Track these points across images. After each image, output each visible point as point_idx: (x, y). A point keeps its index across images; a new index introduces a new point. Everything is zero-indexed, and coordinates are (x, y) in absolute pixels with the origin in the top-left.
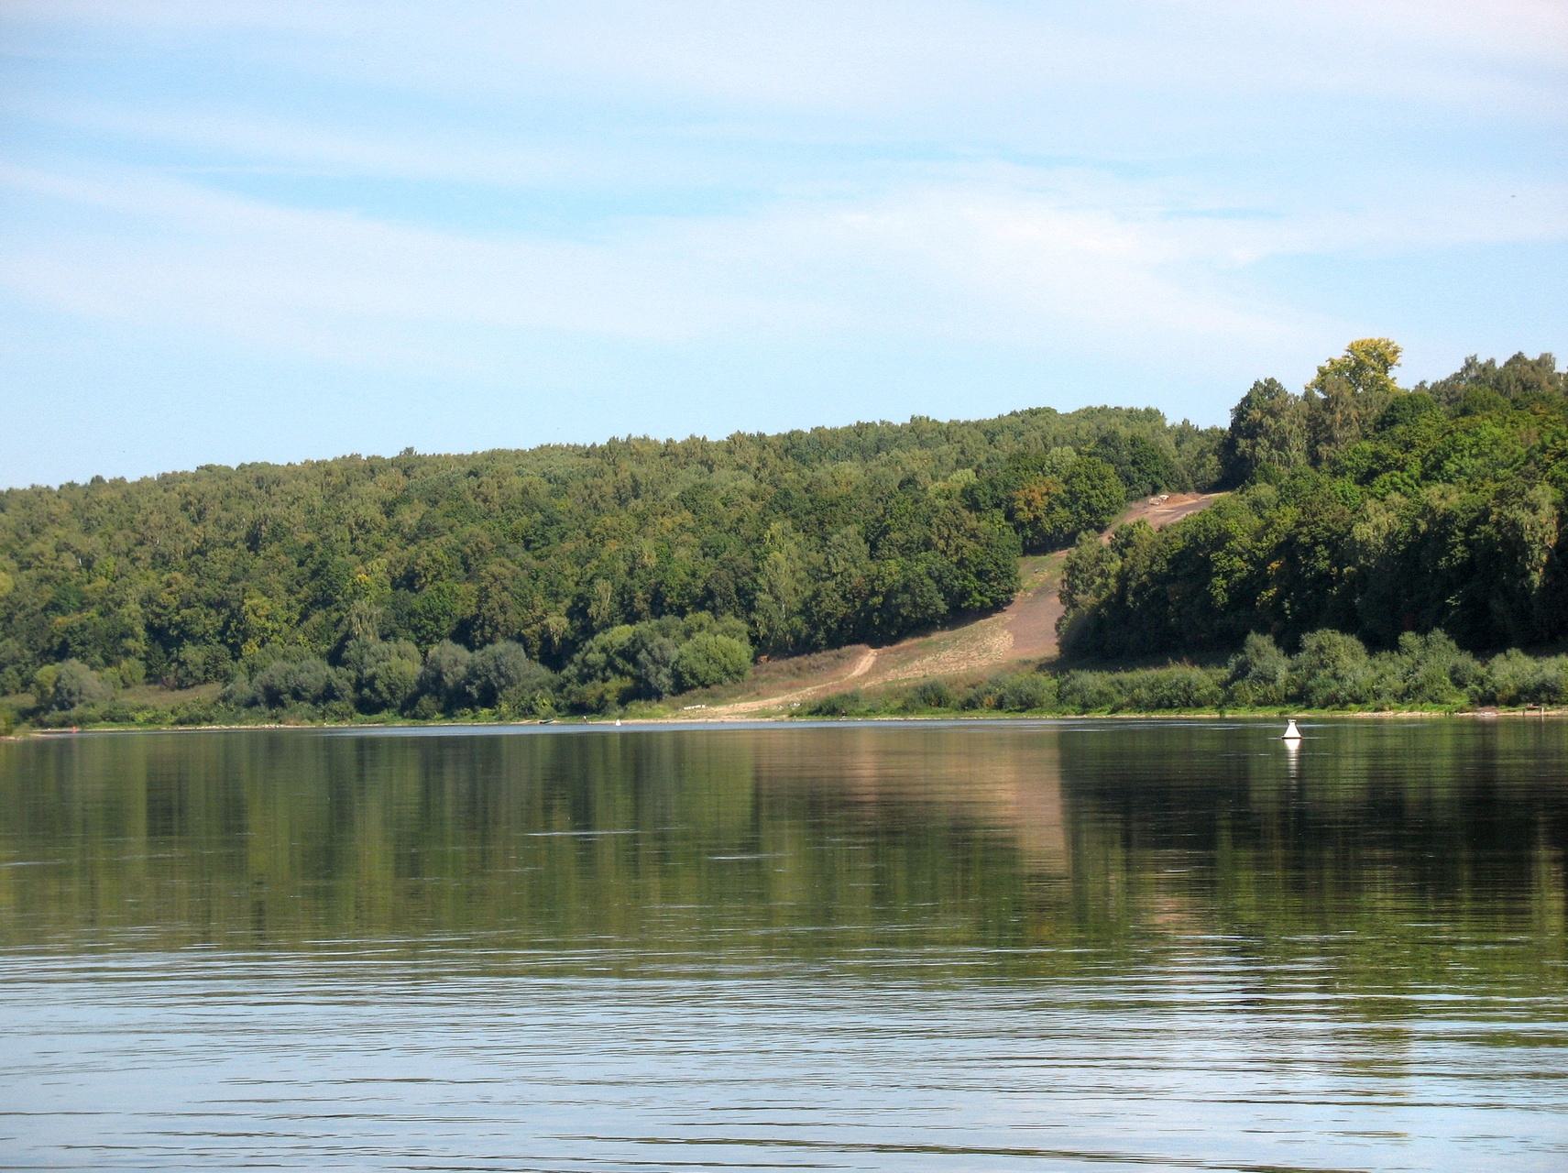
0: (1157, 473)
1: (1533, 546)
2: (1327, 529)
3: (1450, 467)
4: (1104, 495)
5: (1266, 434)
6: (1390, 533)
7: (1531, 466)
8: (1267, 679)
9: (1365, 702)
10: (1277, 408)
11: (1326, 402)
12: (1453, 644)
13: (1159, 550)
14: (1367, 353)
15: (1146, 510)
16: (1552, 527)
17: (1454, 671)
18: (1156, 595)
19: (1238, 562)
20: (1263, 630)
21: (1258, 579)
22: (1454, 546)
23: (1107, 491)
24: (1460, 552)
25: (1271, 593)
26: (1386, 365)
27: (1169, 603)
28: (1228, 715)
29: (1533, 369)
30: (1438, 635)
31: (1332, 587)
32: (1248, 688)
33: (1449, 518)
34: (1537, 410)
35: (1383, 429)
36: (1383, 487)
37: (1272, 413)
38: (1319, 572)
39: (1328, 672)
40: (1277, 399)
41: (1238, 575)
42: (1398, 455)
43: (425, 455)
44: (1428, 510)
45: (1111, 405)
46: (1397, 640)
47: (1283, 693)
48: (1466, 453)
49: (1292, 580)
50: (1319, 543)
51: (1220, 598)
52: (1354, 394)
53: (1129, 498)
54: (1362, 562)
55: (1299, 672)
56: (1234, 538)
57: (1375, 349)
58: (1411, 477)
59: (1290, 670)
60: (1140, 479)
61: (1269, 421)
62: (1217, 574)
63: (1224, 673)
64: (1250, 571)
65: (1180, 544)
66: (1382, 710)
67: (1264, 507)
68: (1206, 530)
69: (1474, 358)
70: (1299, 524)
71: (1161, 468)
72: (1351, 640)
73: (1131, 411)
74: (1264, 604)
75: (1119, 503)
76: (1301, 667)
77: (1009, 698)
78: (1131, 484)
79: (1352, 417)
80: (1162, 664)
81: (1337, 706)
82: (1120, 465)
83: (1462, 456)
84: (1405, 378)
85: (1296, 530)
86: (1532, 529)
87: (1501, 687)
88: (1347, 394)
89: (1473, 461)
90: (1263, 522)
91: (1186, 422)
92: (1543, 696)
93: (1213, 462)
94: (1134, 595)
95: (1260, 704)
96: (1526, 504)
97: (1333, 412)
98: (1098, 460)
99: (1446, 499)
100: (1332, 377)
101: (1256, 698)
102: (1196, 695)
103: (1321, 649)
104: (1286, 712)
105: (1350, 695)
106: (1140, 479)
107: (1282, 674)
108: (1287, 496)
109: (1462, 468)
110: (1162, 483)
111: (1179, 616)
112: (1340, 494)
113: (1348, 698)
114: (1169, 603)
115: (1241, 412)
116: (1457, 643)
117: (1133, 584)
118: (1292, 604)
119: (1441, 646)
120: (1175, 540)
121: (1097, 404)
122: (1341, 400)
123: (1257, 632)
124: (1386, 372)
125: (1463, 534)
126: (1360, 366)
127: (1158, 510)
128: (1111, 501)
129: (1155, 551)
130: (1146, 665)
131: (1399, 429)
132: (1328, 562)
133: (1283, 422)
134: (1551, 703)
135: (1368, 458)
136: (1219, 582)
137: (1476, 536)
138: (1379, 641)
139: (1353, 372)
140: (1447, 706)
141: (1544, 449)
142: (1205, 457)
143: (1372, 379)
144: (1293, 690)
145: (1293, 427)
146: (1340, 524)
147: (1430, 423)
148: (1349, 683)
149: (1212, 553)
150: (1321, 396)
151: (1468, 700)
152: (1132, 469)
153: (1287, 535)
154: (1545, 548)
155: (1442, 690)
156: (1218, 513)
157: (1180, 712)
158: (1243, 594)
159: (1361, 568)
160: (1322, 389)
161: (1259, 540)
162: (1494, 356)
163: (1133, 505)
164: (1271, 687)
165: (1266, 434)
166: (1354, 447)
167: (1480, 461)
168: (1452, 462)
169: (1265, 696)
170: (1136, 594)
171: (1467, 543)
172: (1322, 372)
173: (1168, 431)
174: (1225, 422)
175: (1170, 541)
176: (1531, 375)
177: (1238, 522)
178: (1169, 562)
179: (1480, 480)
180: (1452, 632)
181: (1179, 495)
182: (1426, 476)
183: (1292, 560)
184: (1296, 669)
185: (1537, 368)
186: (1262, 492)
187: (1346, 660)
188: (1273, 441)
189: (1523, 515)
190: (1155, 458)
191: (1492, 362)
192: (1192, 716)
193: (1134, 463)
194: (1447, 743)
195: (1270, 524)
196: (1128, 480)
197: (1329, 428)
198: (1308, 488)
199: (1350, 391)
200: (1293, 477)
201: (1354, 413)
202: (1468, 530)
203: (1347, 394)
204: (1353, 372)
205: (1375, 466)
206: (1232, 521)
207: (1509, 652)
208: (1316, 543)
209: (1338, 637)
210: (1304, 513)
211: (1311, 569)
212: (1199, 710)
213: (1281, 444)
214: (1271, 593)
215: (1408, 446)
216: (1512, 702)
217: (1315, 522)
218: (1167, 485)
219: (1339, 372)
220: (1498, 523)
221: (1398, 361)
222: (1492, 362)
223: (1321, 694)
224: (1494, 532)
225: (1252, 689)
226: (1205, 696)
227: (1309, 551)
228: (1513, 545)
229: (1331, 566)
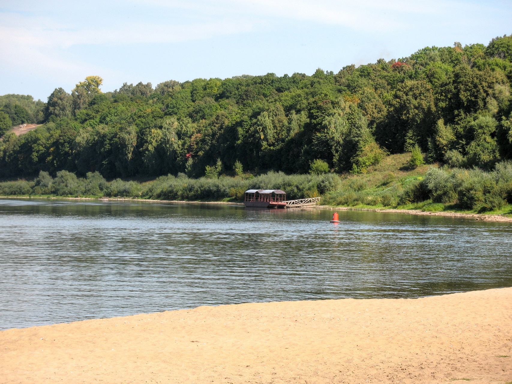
1: (129, 146)
2: (68, 138)
3: (108, 119)
4: (5, 124)
5: (59, 106)
6: (87, 140)
7: (131, 120)
8: (45, 186)
9: (73, 194)
10: (62, 97)
11: (78, 96)
12: (102, 176)
13: (17, 143)
14: (92, 80)
15: (19, 129)
16: (135, 139)
17: (100, 185)
18: (15, 157)
19: (41, 148)
20: (44, 170)
21: (47, 154)
22: (106, 145)
23: (6, 123)
24: (108, 147)
25: (51, 158)
26: (98, 85)
28: (32, 197)
29: (145, 87)
30: (97, 173)
31: (69, 157)
33: (104, 136)
34: (138, 101)
35: (91, 105)
36: (87, 125)
37: (61, 99)
38: (66, 152)
39: (64, 184)
40: (62, 94)
41: (41, 152)
42: (94, 114)
43: (116, 91)
44: (98, 133)
45: (16, 94)
46: (86, 174)
47: (50, 190)
48: (113, 115)
49: (57, 154)
50: (66, 142)
53: (13, 125)
55: (56, 184)
56: (40, 140)
57: (94, 79)
58: (96, 122)
59: (53, 183)
60: (17, 119)
61: (59, 101)
62: (34, 151)
63: (32, 183)
64: (45, 151)
65: (23, 141)
66: (77, 197)
68: (31, 137)
69: (126, 84)
71: (24, 115)
73: (22, 96)
74: (48, 162)
75: (9, 127)
76: (56, 182)
78: (15, 120)
79: (86, 101)
80: (16, 180)
81: (65, 195)
82: (11, 114)
84: (105, 89)
85: (59, 138)
86: (128, 140)
88: (85, 93)
89: (115, 118)
90: (50, 135)
91: (39, 100)
92: (125, 194)
93: (41, 114)
94: (8, 157)
95: (43, 194)
96: (127, 132)
97: (80, 99)
98: (3, 112)
99: (104, 129)
100: (80, 88)
102: (23, 191)
103: (62, 177)
104: (50, 197)
105: (69, 192)
106: (17, 119)
107: (50, 184)
108: (58, 127)
109: (111, 120)
110: (26, 121)
111: (22, 165)
112: (74, 127)
113: (68, 193)
114: (19, 160)
115: (51, 98)
116: (103, 176)
117: (8, 154)
119: (98, 177)
122: (83, 95)
123: (43, 171)
124: (98, 87)
125: (108, 141)
126: (89, 85)
127: (22, 129)
128: (7, 126)
129: (15, 143)
130: (10, 180)
131: (95, 106)
132: (68, 148)
133: (64, 102)
134: (127, 196)
135: (85, 115)
136: (35, 154)
137: (112, 142)
138: (81, 175)
139: (87, 86)
140: (97, 196)
141: (135, 114)
142: (38, 112)
143: (93, 89)
144: (53, 190)
146: (73, 136)
147: (105, 104)
148: (69, 188)
149: (33, 144)
150: (77, 93)
151: (103, 194)
152: (15, 116)
153: (56, 139)
154: (132, 146)
155: (96, 191)
156: (36, 131)
157: (17, 196)
158: (42, 157)
159: (78, 151)
160: (77, 92)
161: (48, 141)
162: (133, 83)
163: (15, 127)
164: (47, 188)
165: (59, 106)
166: (82, 112)
167: (117, 117)
168: (109, 118)
169: (45, 191)
170: (9, 157)
171: (111, 144)
172: (77, 86)
174: (46, 101)
175: (20, 140)
176: (144, 89)
177: (42, 135)
178: (19, 147)
179: (116, 124)
180: (102, 173)
181: (30, 125)
182: (101, 122)
183: (57, 148)
184: (55, 183)
185: (146, 87)
187: (70, 181)
188: (61, 108)
189: (126, 135)
190: (23, 112)
191: (132, 85)
192: (15, 197)
193: (16, 114)
195: (52, 136)
196: (14, 119)
197: (79, 104)
200: (60, 121)
201: (87, 100)
202: (110, 140)
203: (85, 93)
204: (87, 86)
205: (86, 118)
206: (39, 134)
207: (117, 179)
208: (65, 142)
209: (67, 173)
210: (61, 132)
212: (24, 195)
213: (63, 109)
214: (51, 158)
215: (98, 112)
216: (116, 196)
217: (65, 136)
218: (27, 121)
219: (83, 86)
220: (119, 138)
221: (102, 83)
222: (132, 85)
223: (61, 191)
224: (118, 140)
225: (41, 189)
226: (26, 191)
227: (63, 145)
228: (123, 145)
229: (69, 150)
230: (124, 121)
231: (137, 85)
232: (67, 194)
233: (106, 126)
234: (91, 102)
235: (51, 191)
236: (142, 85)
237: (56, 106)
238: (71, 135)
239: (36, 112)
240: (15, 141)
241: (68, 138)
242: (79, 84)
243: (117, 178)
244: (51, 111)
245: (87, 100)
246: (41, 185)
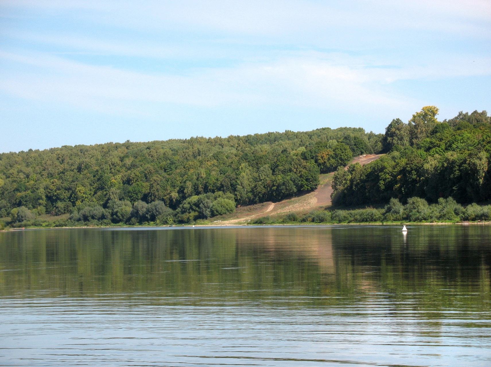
1: (480, 171)
2: (416, 165)
3: (454, 146)
4: (346, 155)
5: (396, 136)
6: (435, 167)
7: (479, 146)
8: (397, 212)
9: (428, 220)
10: (400, 128)
11: (415, 126)
12: (455, 202)
13: (363, 172)
14: (428, 110)
15: (359, 160)
16: (486, 165)
17: (455, 210)
18: (362, 186)
19: (388, 176)
21: (394, 181)
22: (455, 171)
23: (347, 154)
24: (457, 173)
25: (398, 185)
26: (434, 114)
27: (366, 189)
29: (480, 115)
30: (450, 199)
31: (417, 184)
32: (391, 215)
33: (454, 162)
34: (481, 128)
35: (433, 134)
37: (398, 129)
38: (413, 179)
39: (416, 210)
40: (400, 125)
41: (388, 180)
42: (438, 142)
44: (447, 160)
45: (348, 127)
46: (437, 200)
48: (459, 142)
49: (405, 181)
50: (413, 170)
51: (382, 187)
52: (424, 123)
53: (354, 156)
54: (426, 176)
55: (407, 210)
56: (386, 168)
58: (442, 149)
59: (404, 210)
60: (357, 150)
61: (397, 132)
62: (381, 180)
63: (383, 211)
64: (391, 179)
65: (369, 170)
66: (433, 222)
67: (396, 159)
68: (378, 166)
69: (462, 112)
71: (363, 146)
73: (354, 129)
74: (396, 189)
75: (350, 157)
76: (407, 209)
78: (354, 151)
79: (423, 130)
80: (364, 208)
81: (419, 221)
82: (351, 146)
83: (458, 143)
85: (406, 166)
86: (480, 165)
87: (470, 215)
88: (422, 123)
89: (461, 144)
90: (395, 163)
91: (371, 132)
92: (483, 218)
93: (380, 144)
95: (394, 220)
96: (478, 158)
97: (417, 129)
98: (344, 144)
99: (453, 156)
100: (417, 118)
102: (375, 217)
103: (414, 203)
104: (403, 223)
105: (423, 218)
106: (357, 150)
107: (402, 211)
108: (403, 155)
109: (458, 146)
110: (364, 151)
112: (420, 155)
113: (422, 218)
114: (366, 189)
115: (388, 129)
116: (456, 201)
117: (355, 183)
118: (405, 189)
119: (451, 202)
120: (368, 169)
121: (343, 126)
123: (394, 198)
124: (434, 116)
125: (458, 167)
126: (426, 114)
127: (363, 160)
128: (348, 157)
129: (362, 172)
130: (359, 208)
131: (438, 134)
132: (416, 176)
133: (402, 132)
134: (486, 220)
135: (428, 143)
136: (382, 182)
137: (462, 168)
138: (432, 201)
139: (424, 116)
141: (483, 140)
143: (430, 119)
144: (405, 216)
146: (420, 164)
147: (448, 132)
148: (422, 214)
149: (380, 173)
150: (414, 124)
152: (354, 147)
153: (403, 167)
154: (484, 172)
155: (452, 216)
157: (369, 223)
158: (389, 186)
159: (426, 178)
160: (414, 122)
161: (394, 169)
162: (468, 111)
163: (355, 158)
164: (398, 215)
165: (396, 136)
166: (424, 140)
168: (455, 145)
169: (396, 218)
170: (356, 186)
171: (459, 170)
172: (414, 116)
174: (383, 132)
176: (480, 117)
177: (388, 163)
178: (366, 176)
179: (463, 150)
180: (455, 198)
181: (369, 155)
182: (446, 149)
183: (405, 175)
184: (406, 209)
185: (481, 115)
187: (422, 207)
188: (399, 138)
189: (477, 161)
190: (362, 143)
191: (467, 113)
192: (373, 224)
193: (355, 145)
194: (453, 232)
195: (398, 164)
196: (353, 150)
197: (416, 134)
199: (423, 122)
200: (405, 149)
201: (424, 129)
202: (460, 166)
203: (422, 123)
204: (424, 116)
205: (430, 146)
206: (386, 163)
207: (472, 204)
208: (412, 170)
209: (419, 199)
211: (411, 178)
212: (376, 222)
213: (401, 139)
214: (398, 185)
215: (441, 140)
216: (474, 220)
217: (412, 163)
218: (366, 152)
219: (419, 116)
220: (469, 164)
221: (438, 113)
222: (467, 113)
223: (414, 217)
225: (392, 215)
226: (377, 218)
227: (410, 172)
229: (417, 177)
230: (472, 148)
231: (472, 114)
232: (421, 220)
233: (454, 152)
234: (433, 130)
235: (403, 218)
236: (478, 113)
237: (394, 136)
238: (417, 163)
239: (374, 142)
240: (361, 170)
241: (415, 165)
242: (416, 114)
243: (473, 203)
244: (390, 141)
245: (424, 129)
246: (392, 211)
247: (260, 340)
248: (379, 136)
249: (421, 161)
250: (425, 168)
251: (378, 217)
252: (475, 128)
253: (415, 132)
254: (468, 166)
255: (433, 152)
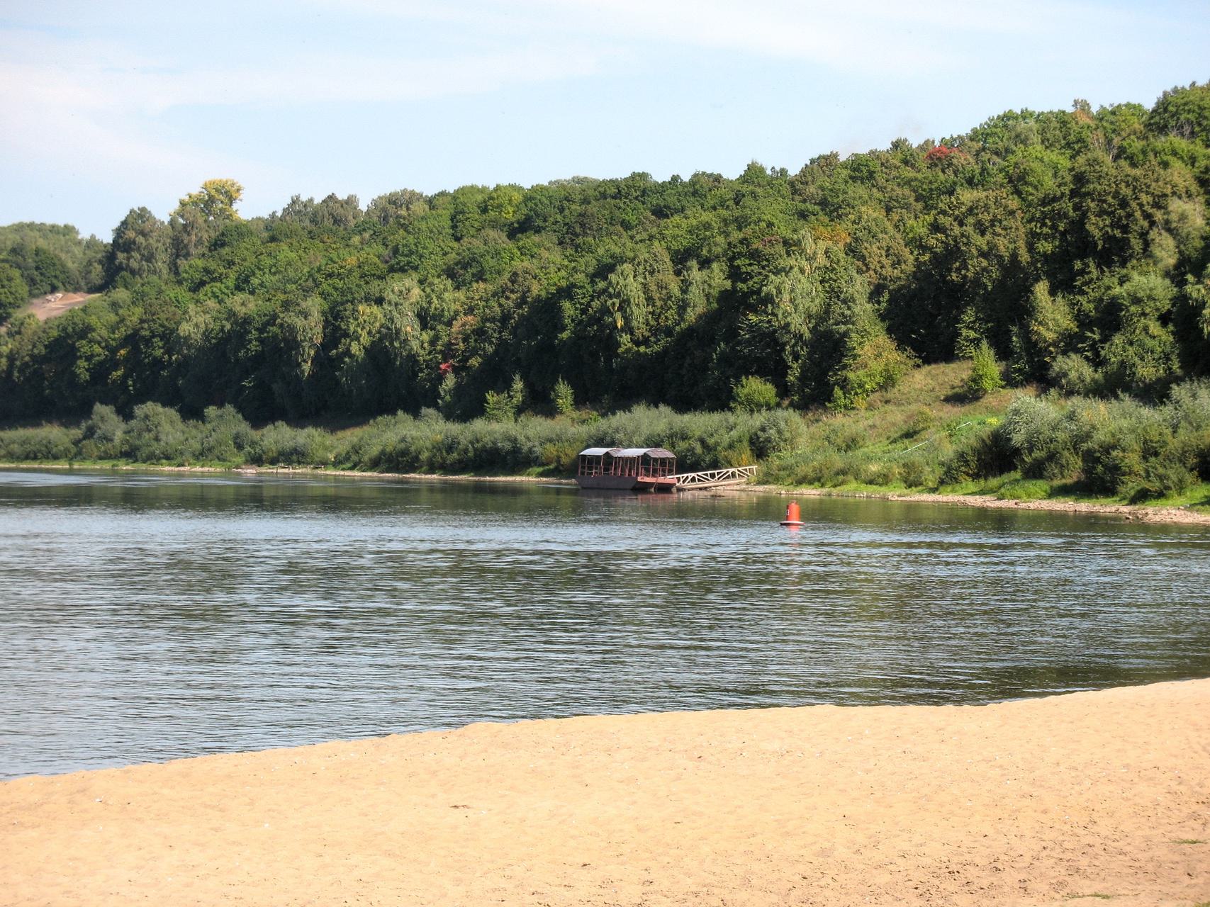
0: (55, 277)
1: (304, 344)
2: (161, 325)
3: (255, 281)
4: (11, 293)
7: (310, 283)
8: (107, 439)
9: (173, 459)
10: (147, 230)
11: (185, 226)
12: (240, 416)
13: (39, 338)
14: (217, 190)
15: (44, 305)
16: (319, 329)
18: (35, 371)
19: (97, 349)
21: (111, 363)
22: (250, 341)
23: (13, 290)
24: (254, 346)
25: (119, 373)
26: (231, 200)
27: (45, 379)
29: (342, 206)
30: (229, 408)
32: (93, 446)
33: (247, 321)
34: (325, 239)
35: (215, 249)
37: (143, 234)
38: (155, 358)
39: (152, 435)
40: (147, 223)
41: (97, 358)
42: (222, 270)
44: (231, 314)
45: (38, 221)
46: (203, 411)
48: (267, 271)
49: (134, 363)
50: (157, 336)
51: (82, 376)
52: (206, 221)
53: (32, 295)
54: (185, 352)
55: (132, 434)
56: (94, 330)
57: (223, 187)
58: (227, 288)
59: (125, 433)
60: (41, 281)
61: (140, 239)
62: (81, 357)
63: (77, 433)
65: (55, 333)
66: (183, 465)
67: (121, 307)
68: (74, 323)
69: (298, 198)
70: (142, 321)
71: (58, 273)
72: (172, 413)
73: (53, 226)
74: (114, 381)
75: (22, 299)
77: (738, 445)
78: (34, 285)
79: (204, 239)
81: (155, 461)
82: (26, 270)
83: (264, 274)
84: (248, 209)
85: (139, 326)
86: (304, 331)
87: (266, 451)
88: (201, 221)
89: (272, 278)
90: (117, 319)
91: (93, 237)
92: (294, 458)
94: (19, 372)
95: (101, 458)
96: (300, 311)
97: (189, 234)
98: (7, 266)
99: (245, 306)
101: (99, 454)
102: (54, 450)
103: (147, 417)
105: (163, 453)
106: (41, 281)
107: (119, 435)
108: (137, 299)
109: (263, 282)
110: (60, 285)
113: (162, 456)
114: (45, 379)
115: (119, 232)
116: (243, 416)
117: (18, 363)
118: (134, 382)
120: (51, 330)
121: (27, 220)
122: (195, 225)
123: (102, 403)
124: (231, 205)
126: (212, 200)
127: (52, 305)
128: (16, 298)
129: (36, 338)
130: (24, 426)
132: (162, 351)
133: (151, 241)
134: (299, 463)
135: (200, 272)
136: (82, 363)
137: (265, 335)
138: (192, 412)
139: (206, 203)
143: (220, 210)
144: (126, 448)
145: (160, 246)
146: (172, 322)
148: (162, 443)
149: (78, 340)
150: (181, 221)
151: (244, 459)
152: (36, 273)
153: (133, 329)
156: (84, 310)
157: (41, 463)
158: (100, 372)
159: (185, 356)
160: (182, 217)
161: (114, 333)
162: (314, 196)
163: (35, 301)
164: (110, 445)
166: (193, 264)
169: (105, 452)
170: (21, 371)
171: (261, 341)
172: (183, 204)
173: (80, 242)
174: (108, 238)
175: (48, 331)
176: (341, 211)
177: (99, 318)
178: (46, 347)
180: (240, 409)
181: (71, 295)
182: (238, 288)
183: (135, 350)
184: (129, 432)
185: (345, 206)
186: (119, 295)
187: (166, 427)
188: (143, 255)
189: (297, 320)
190: (54, 265)
191: (311, 200)
193: (37, 268)
194: (232, 491)
195: (122, 320)
196: (32, 282)
197: (186, 246)
198: (153, 293)
199: (204, 218)
200: (143, 285)
201: (205, 236)
203: (201, 221)
204: (206, 203)
205: (204, 278)
206: (93, 317)
207: (276, 424)
208: (154, 336)
209: (159, 408)
210: (145, 313)
211: (149, 357)
212: (57, 462)
213: (150, 258)
214: (119, 373)
215: (231, 264)
216: (273, 462)
218: (65, 286)
219: (195, 204)
220: (281, 325)
221: (241, 197)
222: (311, 200)
223: (145, 452)
225: (97, 447)
227: (148, 342)
229: (163, 354)
232: (159, 459)
235: (121, 452)
237: (133, 250)
242: (187, 198)
243: (277, 420)
244: (121, 263)
245: (205, 236)
247: (411, 686)
248: (92, 244)
249: (174, 314)
250: (182, 334)
251: (62, 448)
252: (311, 238)
253: (182, 241)
254: (280, 331)
255: (206, 295)
